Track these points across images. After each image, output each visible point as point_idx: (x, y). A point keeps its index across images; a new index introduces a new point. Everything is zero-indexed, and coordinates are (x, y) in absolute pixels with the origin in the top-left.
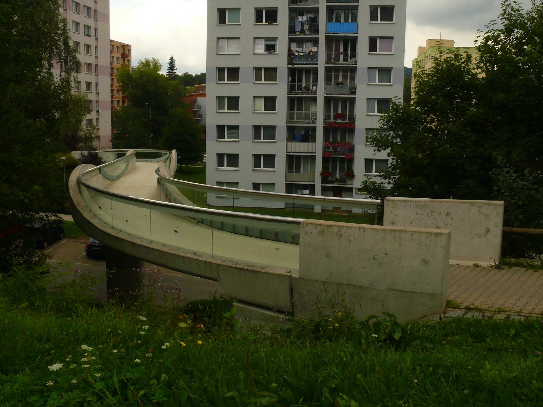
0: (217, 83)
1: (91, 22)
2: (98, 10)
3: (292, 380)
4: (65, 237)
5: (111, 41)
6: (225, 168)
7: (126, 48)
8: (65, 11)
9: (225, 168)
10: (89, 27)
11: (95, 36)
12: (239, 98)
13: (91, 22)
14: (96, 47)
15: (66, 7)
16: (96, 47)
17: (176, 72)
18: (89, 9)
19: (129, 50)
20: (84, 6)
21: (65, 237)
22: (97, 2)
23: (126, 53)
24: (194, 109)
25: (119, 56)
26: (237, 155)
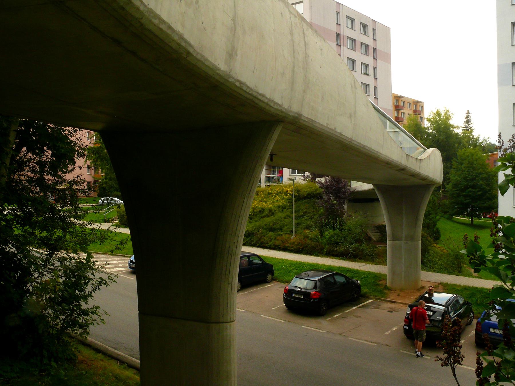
1: (369, 60)
2: (378, 48)
4: (273, 279)
5: (398, 98)
7: (419, 104)
8: (376, 99)
10: (367, 66)
11: (375, 75)
13: (369, 60)
14: (375, 88)
15: (340, 42)
16: (375, 88)
17: (472, 127)
18: (367, 46)
19: (422, 107)
20: (362, 43)
21: (275, 280)
22: (376, 40)
25: (411, 112)
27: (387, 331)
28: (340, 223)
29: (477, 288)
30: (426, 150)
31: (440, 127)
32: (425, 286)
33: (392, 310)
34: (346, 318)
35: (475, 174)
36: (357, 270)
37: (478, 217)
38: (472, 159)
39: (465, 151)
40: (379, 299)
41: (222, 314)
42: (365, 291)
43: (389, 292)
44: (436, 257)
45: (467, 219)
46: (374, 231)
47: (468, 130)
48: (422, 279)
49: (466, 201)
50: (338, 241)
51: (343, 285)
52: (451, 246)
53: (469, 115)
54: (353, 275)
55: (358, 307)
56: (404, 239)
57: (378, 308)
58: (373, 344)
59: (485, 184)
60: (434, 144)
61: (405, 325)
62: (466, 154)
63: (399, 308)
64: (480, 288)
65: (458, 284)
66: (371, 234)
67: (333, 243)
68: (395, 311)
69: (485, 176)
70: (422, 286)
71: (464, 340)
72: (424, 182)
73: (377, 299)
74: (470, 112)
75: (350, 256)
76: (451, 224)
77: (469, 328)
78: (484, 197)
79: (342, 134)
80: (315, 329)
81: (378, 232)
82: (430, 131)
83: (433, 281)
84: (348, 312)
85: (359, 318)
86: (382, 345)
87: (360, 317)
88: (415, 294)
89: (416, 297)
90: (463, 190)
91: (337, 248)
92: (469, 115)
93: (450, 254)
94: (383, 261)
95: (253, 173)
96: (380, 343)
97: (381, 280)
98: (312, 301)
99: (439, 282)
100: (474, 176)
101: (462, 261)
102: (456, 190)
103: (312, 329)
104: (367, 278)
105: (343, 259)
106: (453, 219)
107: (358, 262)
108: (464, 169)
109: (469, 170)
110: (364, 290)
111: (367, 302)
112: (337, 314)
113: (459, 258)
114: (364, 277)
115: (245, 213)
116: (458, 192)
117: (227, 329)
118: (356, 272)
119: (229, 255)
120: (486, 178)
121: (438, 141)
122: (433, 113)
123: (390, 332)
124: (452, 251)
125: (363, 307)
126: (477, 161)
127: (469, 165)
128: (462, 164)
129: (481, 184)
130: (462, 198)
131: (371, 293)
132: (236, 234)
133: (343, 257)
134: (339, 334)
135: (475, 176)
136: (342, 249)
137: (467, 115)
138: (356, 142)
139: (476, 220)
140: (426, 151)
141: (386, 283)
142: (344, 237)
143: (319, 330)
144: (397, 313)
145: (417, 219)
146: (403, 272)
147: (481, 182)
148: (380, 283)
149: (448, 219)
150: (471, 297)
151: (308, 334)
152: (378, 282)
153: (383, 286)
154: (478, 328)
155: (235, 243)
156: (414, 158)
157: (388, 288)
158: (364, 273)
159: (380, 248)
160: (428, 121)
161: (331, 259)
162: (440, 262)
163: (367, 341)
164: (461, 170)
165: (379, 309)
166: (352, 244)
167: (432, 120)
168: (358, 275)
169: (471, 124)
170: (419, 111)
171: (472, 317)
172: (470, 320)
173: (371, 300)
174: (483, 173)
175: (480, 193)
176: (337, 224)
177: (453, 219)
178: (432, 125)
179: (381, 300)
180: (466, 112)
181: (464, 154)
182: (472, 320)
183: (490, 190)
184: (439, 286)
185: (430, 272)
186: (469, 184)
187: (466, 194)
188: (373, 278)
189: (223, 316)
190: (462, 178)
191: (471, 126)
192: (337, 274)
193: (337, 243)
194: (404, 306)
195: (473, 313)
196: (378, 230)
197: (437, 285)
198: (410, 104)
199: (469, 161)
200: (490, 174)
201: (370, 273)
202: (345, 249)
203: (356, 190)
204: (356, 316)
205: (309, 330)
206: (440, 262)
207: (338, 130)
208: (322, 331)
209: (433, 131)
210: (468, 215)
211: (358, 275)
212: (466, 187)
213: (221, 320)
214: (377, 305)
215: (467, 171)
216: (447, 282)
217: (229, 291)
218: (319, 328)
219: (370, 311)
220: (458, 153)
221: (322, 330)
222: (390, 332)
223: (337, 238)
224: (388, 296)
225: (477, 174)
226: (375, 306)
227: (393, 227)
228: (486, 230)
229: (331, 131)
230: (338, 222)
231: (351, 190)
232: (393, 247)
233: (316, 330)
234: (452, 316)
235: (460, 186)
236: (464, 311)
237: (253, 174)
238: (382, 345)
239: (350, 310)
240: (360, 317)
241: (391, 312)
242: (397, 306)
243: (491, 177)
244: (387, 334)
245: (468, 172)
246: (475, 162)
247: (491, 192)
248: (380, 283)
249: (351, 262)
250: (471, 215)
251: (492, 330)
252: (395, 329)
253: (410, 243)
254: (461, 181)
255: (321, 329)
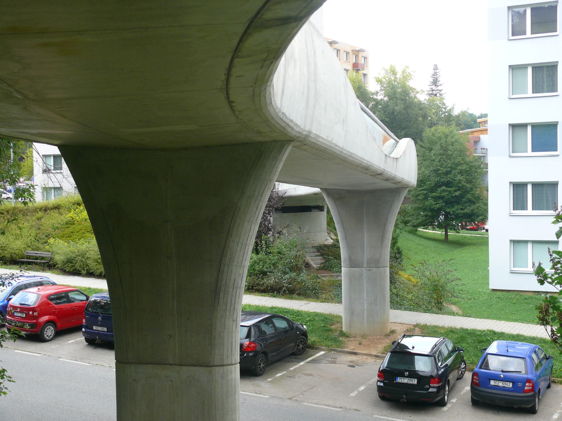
0: (510, 157)
3: (447, 392)
6: (530, 211)
7: (361, 54)
9: (530, 211)
12: (557, 66)
23: (360, 62)
24: (476, 153)
26: (554, 185)
27: (352, 392)
28: (266, 243)
29: (467, 330)
30: (398, 142)
31: (396, 91)
32: (395, 330)
33: (354, 365)
34: (293, 377)
35: (450, 165)
36: (298, 311)
37: (454, 228)
38: (446, 142)
39: (436, 130)
40: (333, 350)
41: (226, 355)
42: (313, 339)
43: (346, 340)
44: (403, 290)
45: (439, 233)
46: (313, 254)
47: (436, 95)
48: (391, 321)
49: (438, 206)
50: (266, 270)
51: (285, 331)
52: (427, 273)
53: (437, 71)
54: (293, 317)
55: (307, 362)
56: (365, 265)
57: (334, 362)
58: (337, 409)
59: (465, 180)
60: (386, 117)
61: (378, 381)
62: (438, 135)
63: (364, 362)
64: (471, 330)
65: (441, 325)
66: (309, 259)
67: (257, 274)
68: (358, 365)
69: (464, 167)
70: (392, 330)
71: (456, 399)
72: (388, 185)
73: (331, 350)
74: (438, 67)
75: (284, 291)
76: (417, 240)
77: (460, 383)
78: (464, 200)
79: (337, 144)
80: (253, 394)
81: (318, 256)
82: (379, 97)
83: (406, 322)
84: (294, 369)
85: (310, 377)
86: (350, 409)
87: (312, 375)
88: (384, 341)
89: (384, 345)
90: (432, 190)
91: (265, 280)
92: (437, 71)
93: (426, 284)
94: (332, 297)
95: (261, 197)
96: (346, 408)
97: (334, 324)
98: (245, 355)
99: (415, 323)
100: (449, 167)
101: (443, 293)
102: (422, 190)
103: (250, 394)
104: (314, 321)
105: (275, 297)
106: (418, 233)
107: (296, 299)
108: (434, 157)
109: (441, 158)
110: (312, 338)
111: (318, 355)
112: (279, 373)
113: (439, 290)
114: (310, 320)
115: (251, 242)
116: (426, 192)
117: (231, 372)
118: (298, 314)
119: (234, 288)
120: (466, 171)
121: (393, 113)
122: (384, 69)
123: (356, 392)
124: (428, 279)
125: (313, 361)
126: (452, 145)
127: (441, 151)
128: (431, 149)
129: (460, 180)
130: (430, 202)
131: (322, 342)
132: (242, 266)
133: (274, 293)
134: (289, 399)
135: (451, 167)
136: (272, 282)
137: (434, 71)
138: (347, 151)
139: (451, 233)
140: (399, 144)
141: (342, 328)
142: (273, 264)
143: (260, 395)
144: (362, 367)
145: (383, 237)
146: (365, 311)
147: (459, 177)
148: (333, 327)
149: (410, 232)
150: (459, 342)
151: (245, 401)
152: (330, 327)
153: (338, 332)
154: (474, 380)
155: (240, 275)
156: (391, 158)
157: (344, 334)
158: (308, 314)
159: (326, 278)
160: (377, 81)
161: (257, 297)
162: (410, 296)
163: (329, 406)
164: (429, 160)
165: (336, 363)
166: (285, 273)
167: (384, 80)
168: (300, 318)
169: (440, 85)
170: (361, 64)
171: (463, 369)
172: (462, 373)
173: (322, 353)
174: (462, 164)
175: (457, 193)
176: (262, 246)
177: (418, 233)
178: (382, 88)
179: (337, 351)
180: (432, 67)
181: (433, 135)
182: (463, 373)
183: (471, 189)
184: (414, 329)
185: (399, 311)
186: (442, 180)
187: (438, 195)
188: (323, 321)
189: (227, 358)
190: (431, 171)
191: (440, 89)
192: (274, 316)
193: (264, 274)
194: (369, 358)
195: (465, 364)
196: (319, 251)
197: (412, 327)
198: (347, 54)
199: (441, 146)
200: (473, 164)
201: (317, 314)
202: (277, 281)
203: (286, 195)
204: (306, 374)
205: (246, 395)
206: (410, 296)
207: (334, 142)
208: (264, 396)
209: (385, 97)
210: (440, 226)
211: (300, 318)
212: (438, 185)
213: (225, 363)
214: (331, 358)
215: (438, 160)
216: (425, 323)
217: (234, 328)
218: (259, 393)
219: (324, 366)
220: (424, 134)
221: (264, 395)
222: (356, 392)
223: (263, 266)
224: (346, 345)
225: (453, 166)
226: (330, 359)
227: (350, 247)
228: (467, 247)
229: (327, 143)
230: (263, 242)
231: (280, 195)
232: (351, 278)
233: (255, 395)
234: (441, 366)
235: (427, 183)
236: (454, 361)
237: (261, 198)
238: (350, 409)
239: (297, 366)
240: (312, 375)
241: (353, 366)
242: (359, 358)
243: (473, 169)
244: (354, 395)
245: (439, 161)
246: (450, 148)
247: (473, 192)
248: (333, 327)
249: (285, 300)
250: (445, 226)
251: (492, 383)
252: (362, 388)
253: (374, 270)
254: (429, 176)
255: (262, 393)
